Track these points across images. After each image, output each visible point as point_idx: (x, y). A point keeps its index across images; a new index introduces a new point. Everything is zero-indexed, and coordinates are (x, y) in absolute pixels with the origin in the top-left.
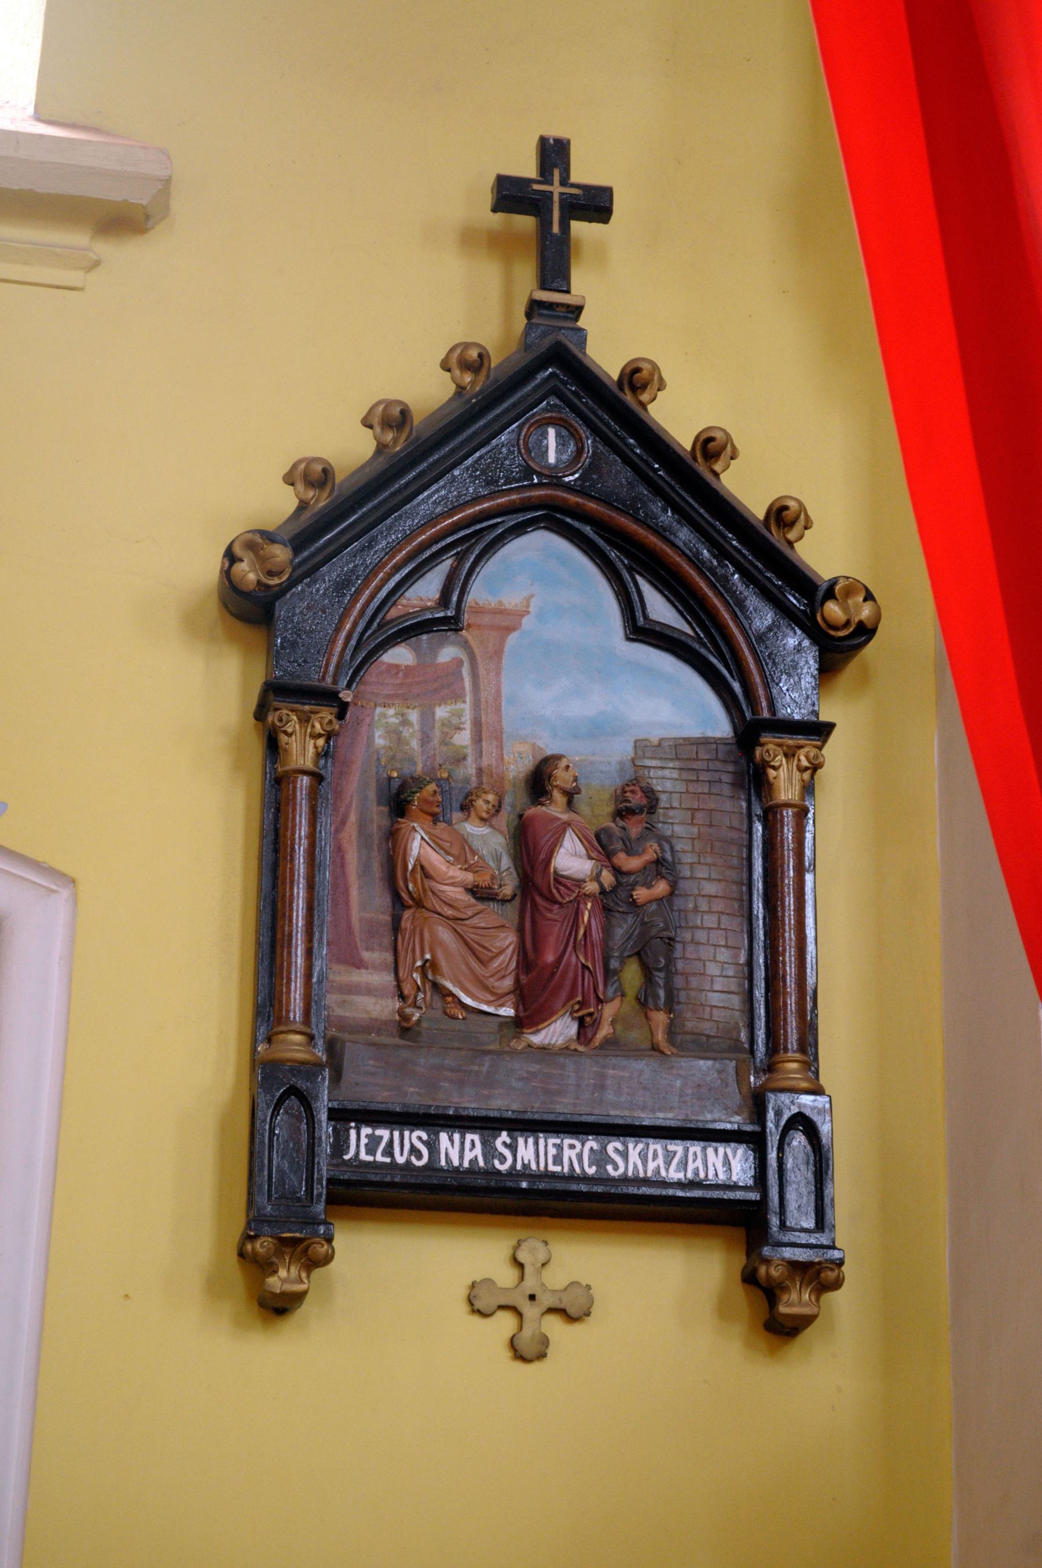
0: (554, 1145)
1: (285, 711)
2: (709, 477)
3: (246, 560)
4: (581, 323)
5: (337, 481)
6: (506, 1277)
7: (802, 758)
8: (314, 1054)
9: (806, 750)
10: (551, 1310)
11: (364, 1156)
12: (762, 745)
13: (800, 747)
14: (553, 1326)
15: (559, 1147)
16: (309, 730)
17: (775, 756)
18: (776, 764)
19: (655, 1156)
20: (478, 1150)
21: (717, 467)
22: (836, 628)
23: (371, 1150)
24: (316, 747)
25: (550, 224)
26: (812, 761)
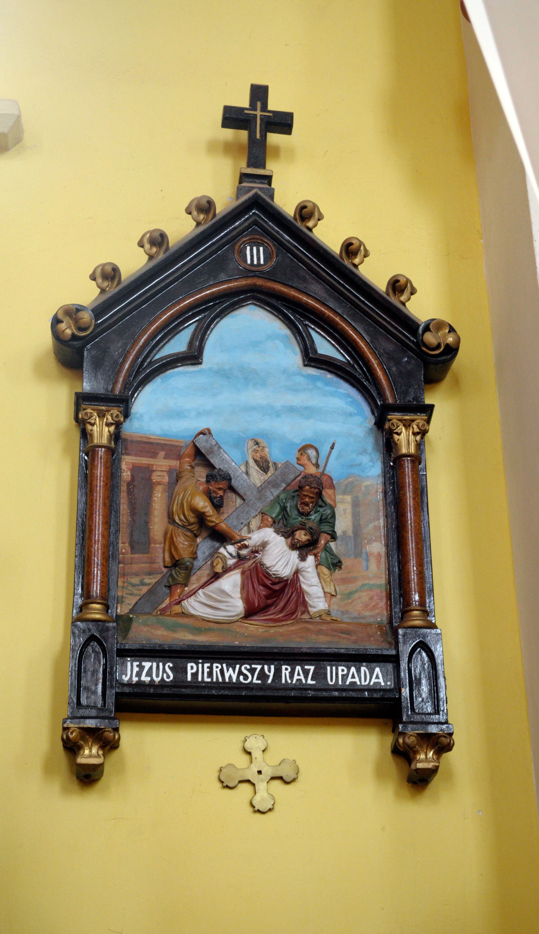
1: (89, 411)
3: (65, 322)
7: (415, 427)
10: (273, 778)
12: (390, 420)
13: (413, 421)
15: (211, 668)
17: (398, 427)
18: (93, 421)
24: (109, 432)
25: (255, 132)
26: (421, 428)
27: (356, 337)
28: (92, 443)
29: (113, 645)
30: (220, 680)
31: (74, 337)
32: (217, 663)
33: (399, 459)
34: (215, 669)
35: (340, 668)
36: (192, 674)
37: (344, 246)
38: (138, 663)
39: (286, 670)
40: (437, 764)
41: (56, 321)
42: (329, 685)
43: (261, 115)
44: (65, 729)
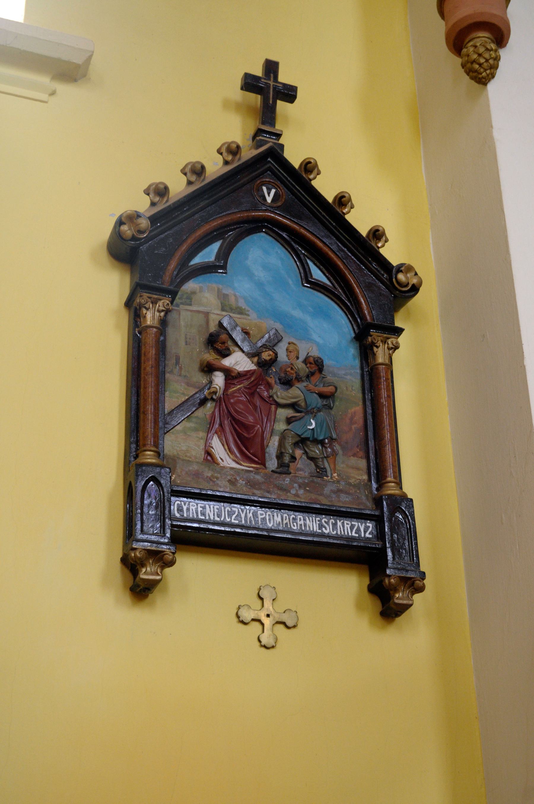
4: (281, 141)
7: (389, 343)
9: (162, 301)
15: (343, 523)
17: (147, 303)
19: (300, 520)
23: (230, 515)
28: (145, 324)
30: (350, 534)
31: (134, 238)
33: (144, 330)
41: (120, 222)
43: (273, 85)
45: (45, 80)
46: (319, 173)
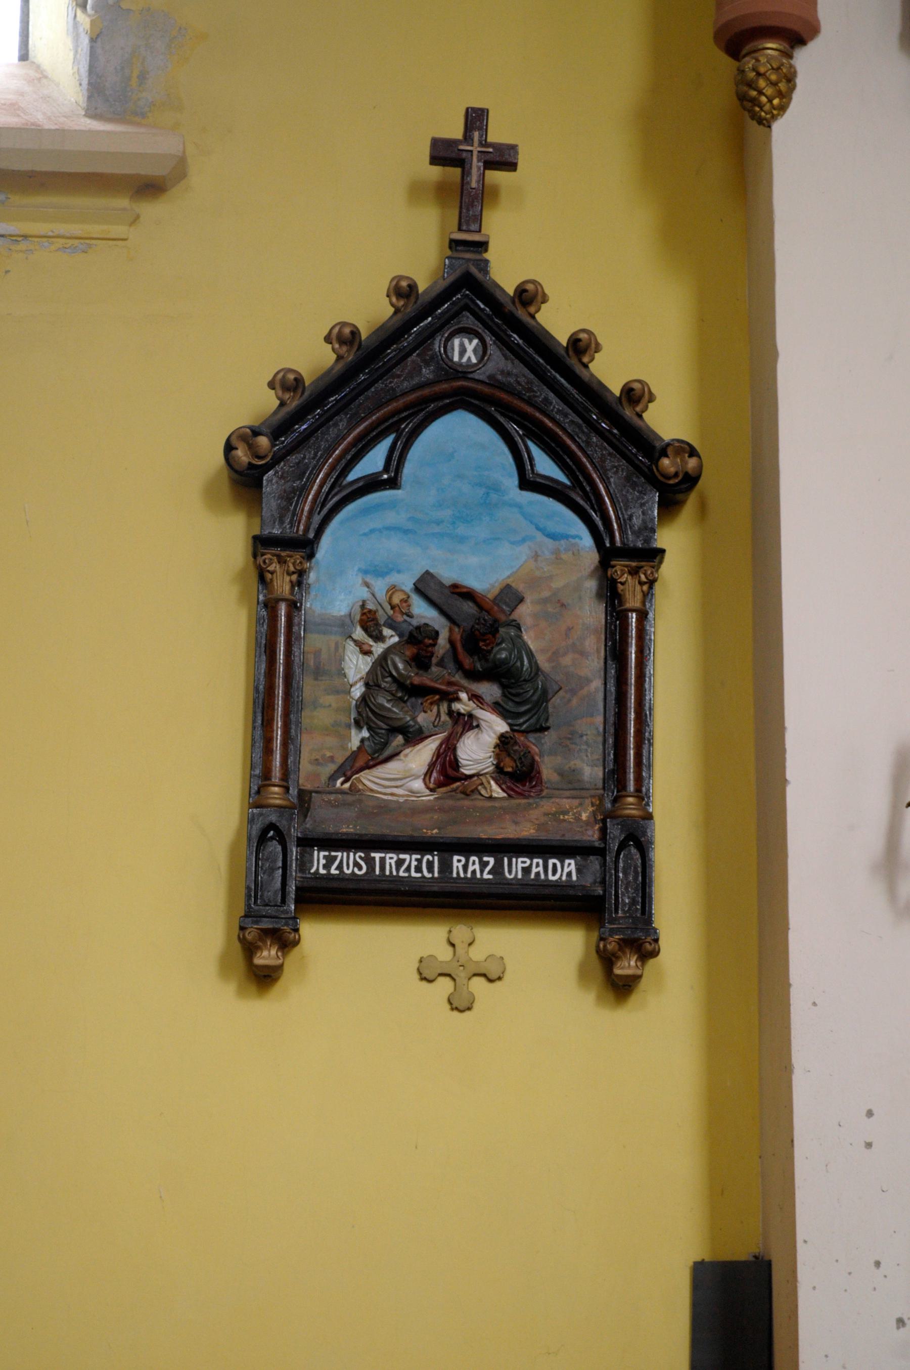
0: (417, 860)
2: (526, 319)
5: (307, 384)
6: (444, 954)
8: (289, 800)
11: (322, 871)
12: (613, 566)
13: (642, 567)
14: (478, 984)
16: (286, 569)
18: (623, 580)
19: (474, 863)
20: (541, 869)
21: (585, 360)
22: (669, 478)
27: (633, 706)
29: (295, 832)
30: (395, 873)
31: (251, 466)
32: (537, 858)
34: (388, 861)
35: (520, 860)
36: (523, 868)
37: (571, 342)
38: (327, 853)
39: (457, 862)
40: (639, 972)
41: (229, 448)
42: (506, 879)
44: (242, 928)
45: (123, 202)
46: (545, 299)
